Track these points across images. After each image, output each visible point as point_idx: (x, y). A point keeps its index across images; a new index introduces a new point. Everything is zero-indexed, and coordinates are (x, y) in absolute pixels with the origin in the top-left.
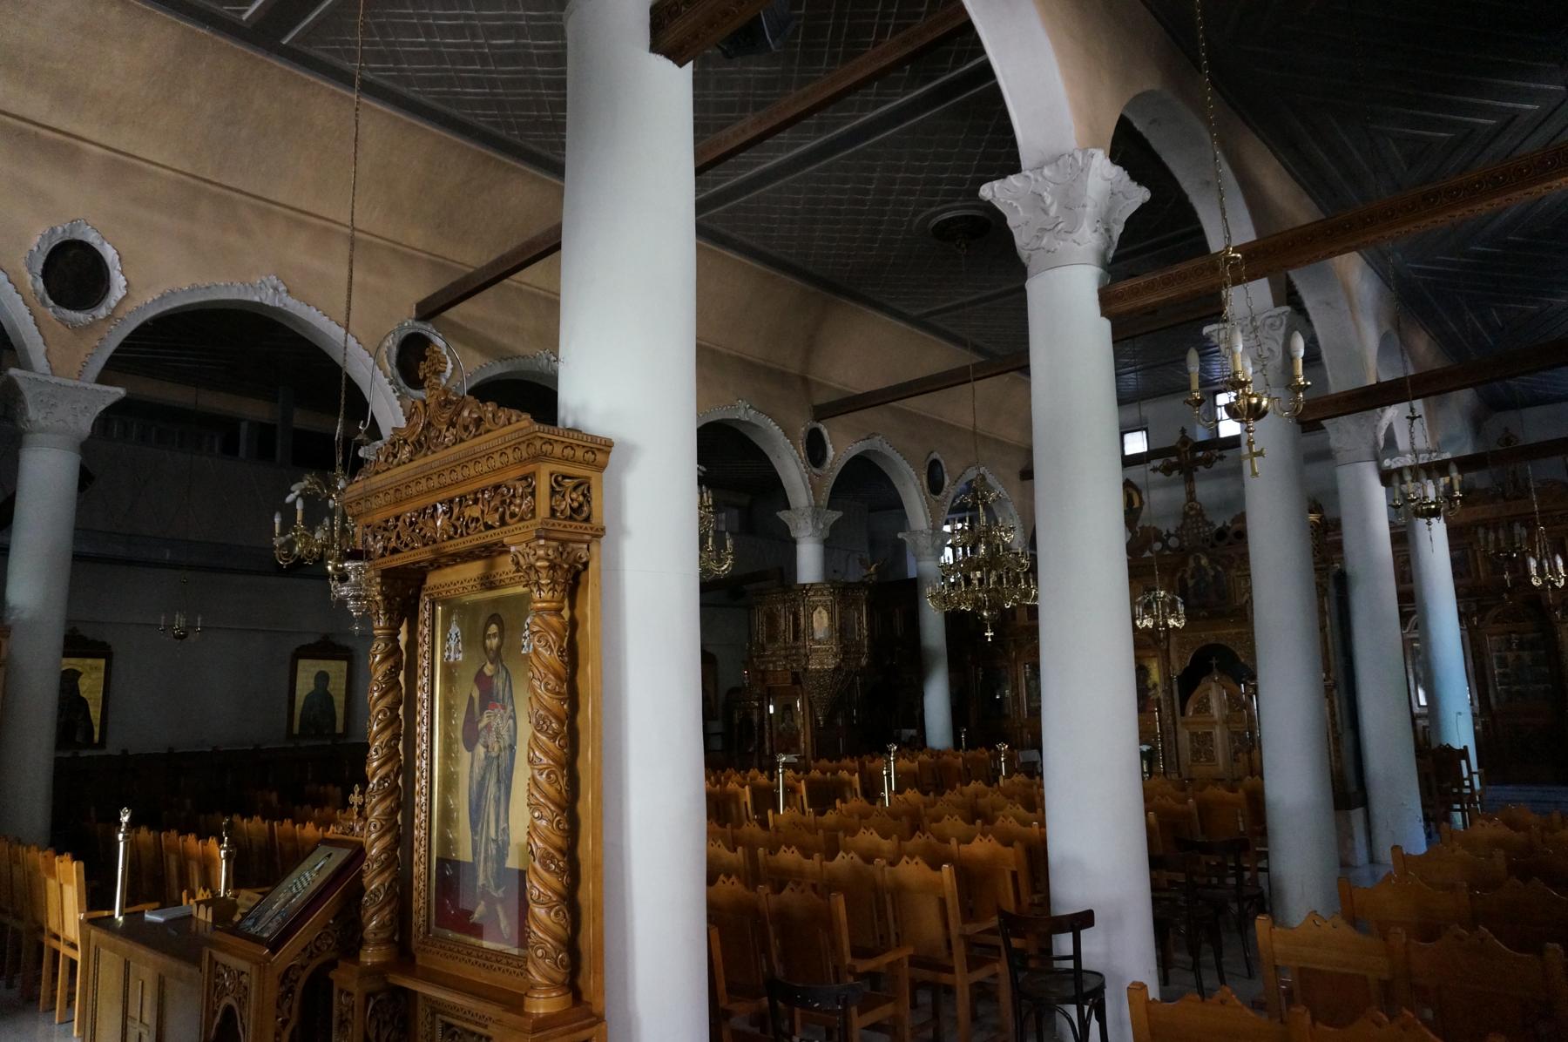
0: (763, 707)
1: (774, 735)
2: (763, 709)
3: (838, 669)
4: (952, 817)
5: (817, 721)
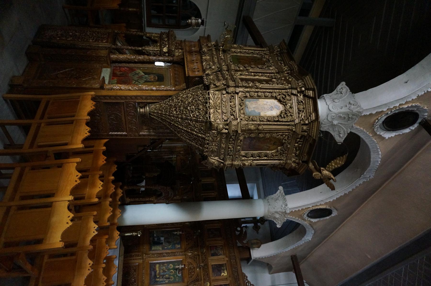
0: (160, 56)
1: (132, 65)
2: (160, 55)
3: (209, 126)
4: (120, 213)
5: (144, 105)
